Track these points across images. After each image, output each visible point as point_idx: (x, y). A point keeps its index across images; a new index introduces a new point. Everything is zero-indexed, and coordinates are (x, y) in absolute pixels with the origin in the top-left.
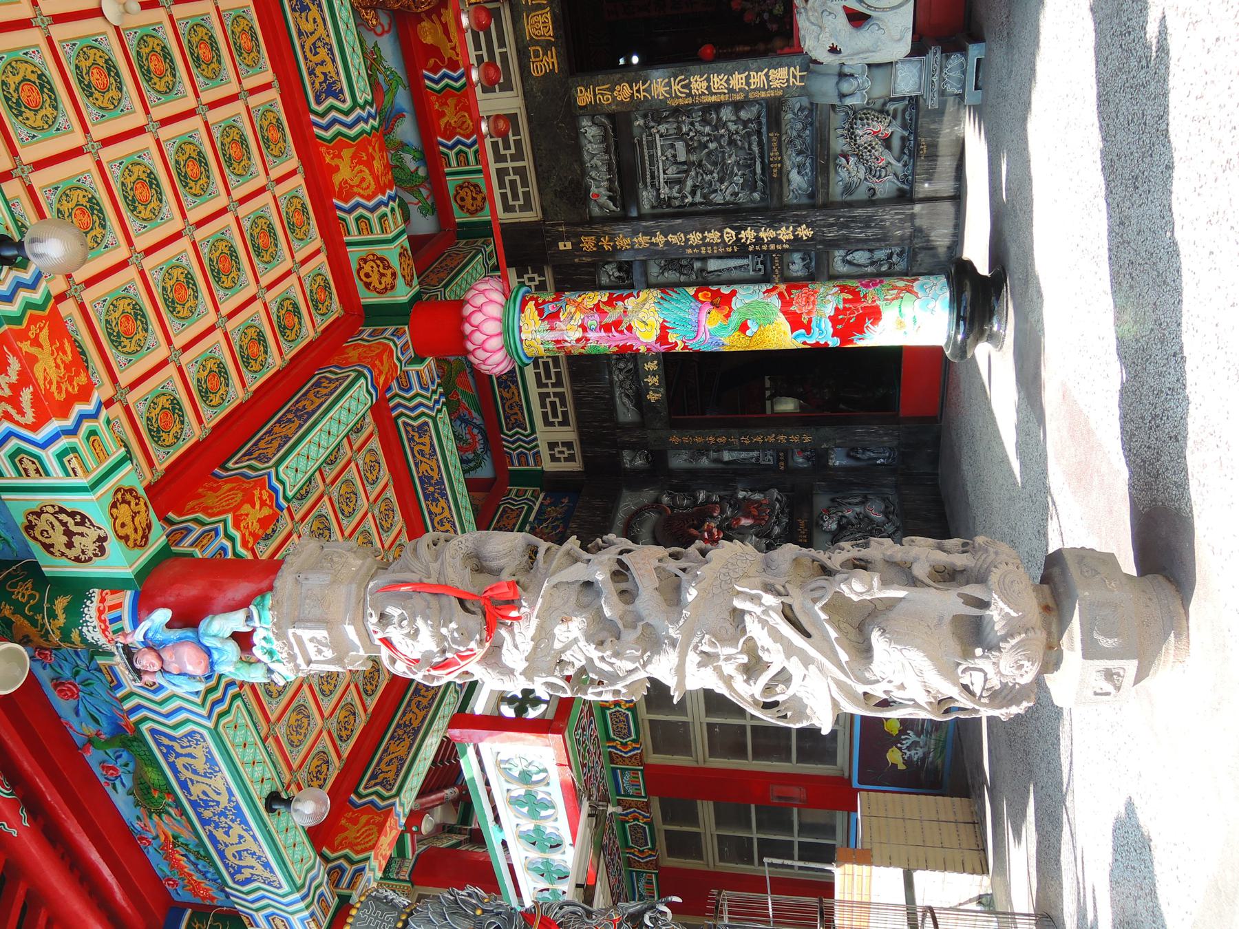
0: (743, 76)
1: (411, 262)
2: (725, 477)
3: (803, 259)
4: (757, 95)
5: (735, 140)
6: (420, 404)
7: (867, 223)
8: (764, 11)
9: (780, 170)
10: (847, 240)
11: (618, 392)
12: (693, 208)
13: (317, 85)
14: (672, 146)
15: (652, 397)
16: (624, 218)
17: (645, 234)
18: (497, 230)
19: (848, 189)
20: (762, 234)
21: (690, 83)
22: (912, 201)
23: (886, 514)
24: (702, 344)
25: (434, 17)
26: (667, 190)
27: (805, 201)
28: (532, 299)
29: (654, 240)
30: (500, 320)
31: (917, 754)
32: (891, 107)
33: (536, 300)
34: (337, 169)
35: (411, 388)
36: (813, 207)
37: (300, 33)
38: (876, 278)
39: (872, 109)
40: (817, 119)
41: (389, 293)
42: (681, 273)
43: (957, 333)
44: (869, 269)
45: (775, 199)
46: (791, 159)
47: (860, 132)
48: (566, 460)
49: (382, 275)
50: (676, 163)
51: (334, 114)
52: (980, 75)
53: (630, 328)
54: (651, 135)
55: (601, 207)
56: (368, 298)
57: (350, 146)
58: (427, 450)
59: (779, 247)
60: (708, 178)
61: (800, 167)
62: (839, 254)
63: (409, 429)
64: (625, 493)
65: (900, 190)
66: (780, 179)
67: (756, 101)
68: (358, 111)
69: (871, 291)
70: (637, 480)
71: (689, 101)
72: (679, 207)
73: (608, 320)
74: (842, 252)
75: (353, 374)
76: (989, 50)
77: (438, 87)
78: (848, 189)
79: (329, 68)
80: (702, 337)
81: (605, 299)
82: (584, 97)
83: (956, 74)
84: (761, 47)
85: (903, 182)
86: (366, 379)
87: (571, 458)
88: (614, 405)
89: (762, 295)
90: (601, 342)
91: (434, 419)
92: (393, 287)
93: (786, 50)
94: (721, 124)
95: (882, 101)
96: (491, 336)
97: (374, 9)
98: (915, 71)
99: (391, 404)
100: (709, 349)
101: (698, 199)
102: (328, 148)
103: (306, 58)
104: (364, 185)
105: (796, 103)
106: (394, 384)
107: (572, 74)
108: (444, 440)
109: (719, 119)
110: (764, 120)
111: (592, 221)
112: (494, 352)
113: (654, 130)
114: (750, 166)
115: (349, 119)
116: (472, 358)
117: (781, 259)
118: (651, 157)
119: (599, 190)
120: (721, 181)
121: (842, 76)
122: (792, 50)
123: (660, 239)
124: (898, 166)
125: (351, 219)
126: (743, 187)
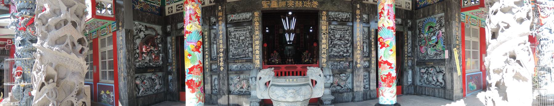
2: (165, 51)
10: (220, 79)
16: (226, 23)
19: (232, 79)
22: (228, 94)
23: (157, 89)
24: (186, 43)
31: (103, 97)
36: (228, 71)
38: (204, 90)
46: (239, 65)
53: (190, 23)
62: (217, 77)
64: (161, 27)
70: (164, 29)
73: (192, 16)
78: (232, 79)
82: (256, 14)
87: (169, 13)
94: (248, 48)
101: (231, 42)
107: (262, 11)
111: (226, 15)
114: (238, 55)
119: (233, 17)
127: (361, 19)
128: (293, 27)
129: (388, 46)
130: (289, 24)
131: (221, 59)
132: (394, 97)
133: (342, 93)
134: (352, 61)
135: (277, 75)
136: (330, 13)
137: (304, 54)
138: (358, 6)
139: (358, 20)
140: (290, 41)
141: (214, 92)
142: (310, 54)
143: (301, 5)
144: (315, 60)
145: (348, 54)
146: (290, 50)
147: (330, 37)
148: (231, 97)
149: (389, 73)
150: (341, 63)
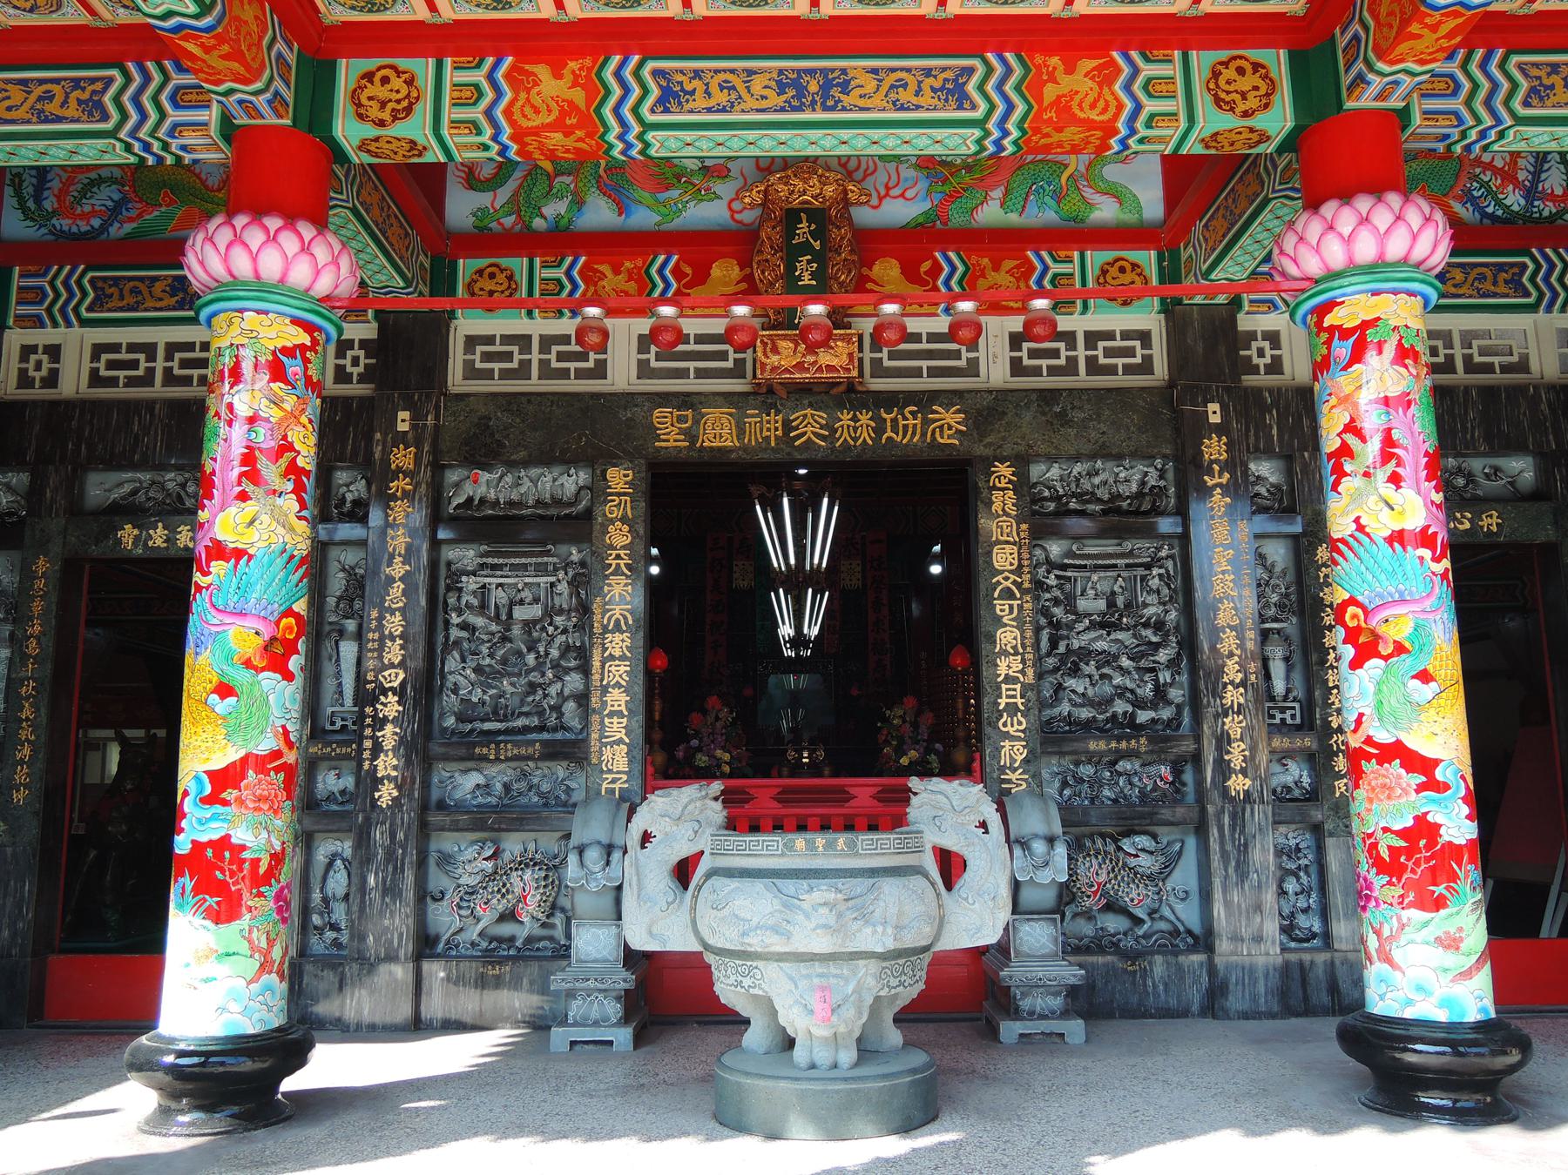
0: (623, 708)
1: (399, 159)
3: (343, 792)
4: (595, 726)
5: (534, 693)
7: (391, 890)
8: (701, 740)
9: (484, 758)
11: (145, 476)
13: (679, 78)
14: (536, 600)
15: (128, 534)
16: (436, 518)
17: (409, 548)
18: (441, 303)
20: (389, 728)
21: (622, 632)
24: (201, 616)
25: (744, 286)
26: (473, 587)
27: (435, 795)
28: (315, 342)
29: (398, 559)
30: (282, 280)
33: (313, 348)
34: (558, 75)
35: (176, 106)
36: (424, 807)
39: (558, 893)
40: (555, 811)
41: (351, 109)
42: (340, 598)
43: (182, 1054)
44: (316, 896)
45: (442, 750)
46: (500, 775)
47: (528, 875)
48: (23, 373)
49: (383, 104)
50: (512, 604)
52: (591, 1047)
53: (243, 497)
54: (556, 569)
55: (457, 485)
56: (348, 72)
57: (589, 103)
58: (52, 108)
59: (366, 755)
60: (485, 650)
61: (486, 788)
62: (346, 847)
63: (99, 86)
65: (437, 938)
66: (471, 757)
67: (586, 725)
69: (268, 904)
71: (597, 629)
72: (445, 602)
74: (348, 853)
76: (623, 1056)
78: (446, 860)
79: (700, 102)
80: (214, 617)
81: (300, 462)
82: (618, 478)
83: (595, 1013)
84: (657, 736)
85: (448, 942)
86: (196, 17)
88: (120, 468)
89: (279, 723)
90: (225, 446)
91: (112, 134)
92: (361, 117)
93: (650, 769)
94: (560, 672)
95: (568, 906)
96: (254, 260)
97: (763, 205)
98: (605, 953)
99: (150, 65)
100: (191, 629)
102: (590, 70)
103: (717, 71)
104: (528, 110)
105: (577, 783)
106: (189, 79)
109: (568, 671)
110: (559, 736)
111: (438, 468)
112: (226, 260)
113: (561, 575)
114: (495, 715)
115: (626, 111)
116: (218, 220)
117: (347, 757)
118: (525, 567)
120: (478, 670)
121: (609, 849)
122: (649, 777)
123: (398, 569)
124: (473, 934)
125: (478, 76)
126: (465, 701)
127: (1240, 486)
128: (819, 556)
129: (1400, 649)
130: (798, 537)
131: (389, 735)
132: (1467, 974)
133: (1133, 956)
134: (1197, 759)
135: (732, 825)
136: (1036, 471)
137: (896, 715)
139: (1219, 500)
140: (798, 641)
141: (317, 945)
142: (927, 719)
143: (866, 436)
144: (960, 756)
145: (1166, 713)
146: (795, 698)
147: (1045, 612)
148: (436, 971)
149: (1420, 820)
150: (1123, 765)
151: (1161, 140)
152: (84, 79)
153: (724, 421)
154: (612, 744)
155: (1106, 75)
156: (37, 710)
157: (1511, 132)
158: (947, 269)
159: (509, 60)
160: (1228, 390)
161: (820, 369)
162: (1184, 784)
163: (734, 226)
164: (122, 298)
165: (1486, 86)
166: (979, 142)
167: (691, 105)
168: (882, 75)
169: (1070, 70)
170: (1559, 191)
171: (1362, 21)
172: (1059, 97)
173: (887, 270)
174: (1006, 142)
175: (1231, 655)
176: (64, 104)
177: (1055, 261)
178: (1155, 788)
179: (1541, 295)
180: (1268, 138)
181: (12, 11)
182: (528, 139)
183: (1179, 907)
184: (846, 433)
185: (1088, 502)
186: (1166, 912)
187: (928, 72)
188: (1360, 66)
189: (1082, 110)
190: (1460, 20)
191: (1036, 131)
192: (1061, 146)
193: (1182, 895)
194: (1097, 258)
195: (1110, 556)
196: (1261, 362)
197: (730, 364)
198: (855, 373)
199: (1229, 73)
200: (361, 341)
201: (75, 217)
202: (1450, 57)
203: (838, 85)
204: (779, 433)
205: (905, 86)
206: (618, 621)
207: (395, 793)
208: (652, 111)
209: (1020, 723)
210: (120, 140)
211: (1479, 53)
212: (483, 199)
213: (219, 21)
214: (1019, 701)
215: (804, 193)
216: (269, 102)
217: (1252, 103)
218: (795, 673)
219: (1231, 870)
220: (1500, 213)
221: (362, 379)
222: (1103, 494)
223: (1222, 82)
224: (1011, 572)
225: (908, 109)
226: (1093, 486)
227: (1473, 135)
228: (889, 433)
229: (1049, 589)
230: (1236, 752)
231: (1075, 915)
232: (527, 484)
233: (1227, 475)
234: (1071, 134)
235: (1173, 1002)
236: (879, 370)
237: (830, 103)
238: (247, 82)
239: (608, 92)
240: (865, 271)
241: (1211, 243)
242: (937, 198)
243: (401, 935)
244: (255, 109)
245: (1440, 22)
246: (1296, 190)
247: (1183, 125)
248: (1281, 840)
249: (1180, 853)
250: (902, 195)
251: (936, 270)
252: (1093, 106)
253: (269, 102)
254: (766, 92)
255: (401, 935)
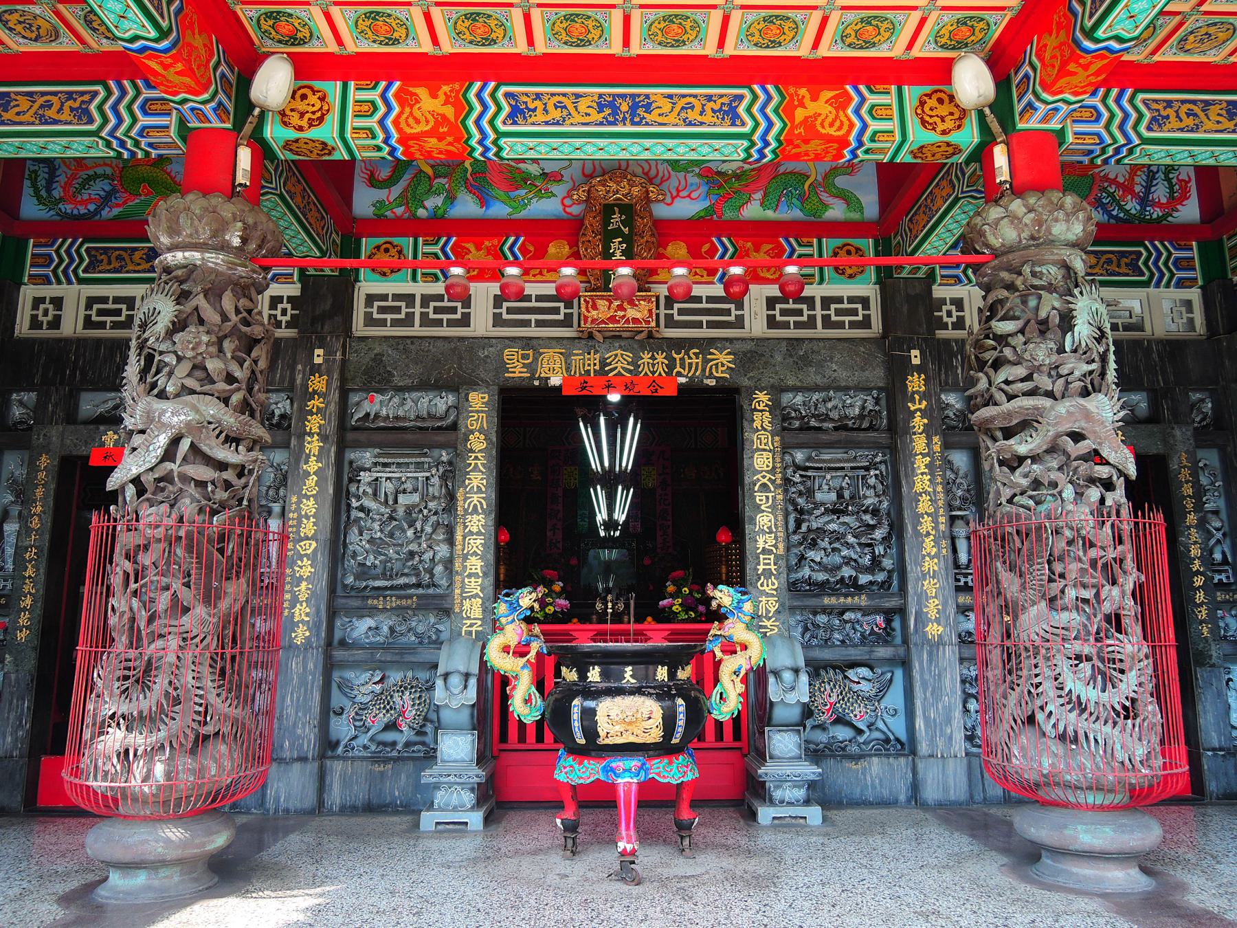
0: (479, 571)
1: (314, 157)
4: (458, 585)
6: (120, 121)
12: (344, 507)
13: (525, 99)
14: (415, 490)
20: (304, 585)
27: (338, 635)
29: (313, 458)
32: (429, 728)
34: (434, 95)
36: (329, 643)
37: (578, 96)
48: (34, 318)
49: (302, 115)
50: (397, 493)
51: (493, 108)
54: (430, 468)
55: (358, 404)
58: (51, 113)
68: (492, 136)
71: (460, 511)
75: (165, 25)
77: (506, 249)
79: (540, 117)
82: (478, 400)
83: (454, 800)
86: (156, 41)
87: (35, 324)
92: (285, 124)
99: (126, 83)
103: (553, 95)
104: (411, 121)
108: (64, 141)
109: (438, 543)
110: (431, 591)
113: (434, 471)
114: (384, 576)
119: (377, 405)
120: (371, 541)
124: (364, 739)
125: (374, 95)
128: (627, 460)
130: (611, 448)
138: (915, 357)
140: (610, 524)
145: (880, 577)
146: (608, 567)
147: (793, 502)
151: (882, 151)
152: (76, 92)
153: (556, 358)
154: (470, 598)
155: (841, 103)
156: (38, 570)
157: (1138, 149)
158: (721, 250)
159: (397, 84)
160: (925, 340)
161: (627, 321)
162: (893, 630)
163: (565, 216)
164: (110, 263)
165: (1119, 115)
166: (747, 150)
167: (533, 119)
168: (675, 99)
169: (815, 98)
170: (1164, 200)
171: (1031, 64)
172: (806, 118)
173: (678, 249)
174: (766, 151)
175: (928, 534)
176: (60, 110)
177: (800, 245)
178: (872, 632)
179: (1152, 275)
180: (960, 151)
181: (21, 40)
182: (411, 143)
183: (889, 720)
184: (646, 369)
185: (823, 421)
186: (881, 725)
187: (709, 98)
188: (1029, 96)
189: (823, 127)
190: (1105, 62)
191: (789, 142)
192: (807, 155)
193: (892, 712)
194: (830, 244)
195: (840, 461)
196: (949, 321)
197: (561, 317)
198: (653, 324)
199: (932, 102)
200: (288, 297)
201: (77, 203)
202: (1094, 94)
203: (643, 106)
204: (597, 367)
205: (692, 108)
206: (475, 506)
207: (307, 634)
208: (504, 123)
209: (773, 584)
210: (101, 138)
211: (1115, 92)
212: (382, 194)
213: (174, 45)
214: (773, 567)
215: (617, 192)
216: (215, 110)
217: (949, 124)
218: (608, 548)
219: (928, 694)
220: (1122, 215)
221: (289, 325)
222: (834, 415)
223: (926, 108)
224: (767, 472)
225: (695, 125)
226: (827, 409)
227: (1110, 151)
228: (678, 369)
229: (795, 483)
230: (932, 606)
231: (814, 727)
232: (409, 403)
233: (924, 403)
234: (815, 146)
235: (886, 793)
236: (670, 322)
237: (637, 119)
238: (197, 94)
239: (471, 109)
240: (661, 250)
241: (914, 232)
242: (714, 198)
243: (309, 741)
244: (204, 115)
245: (1091, 63)
246: (980, 192)
247: (898, 138)
248: (965, 672)
249: (891, 680)
250: (689, 196)
251: (713, 250)
252: (831, 125)
253: (215, 110)
254: (589, 111)
255: (309, 741)
